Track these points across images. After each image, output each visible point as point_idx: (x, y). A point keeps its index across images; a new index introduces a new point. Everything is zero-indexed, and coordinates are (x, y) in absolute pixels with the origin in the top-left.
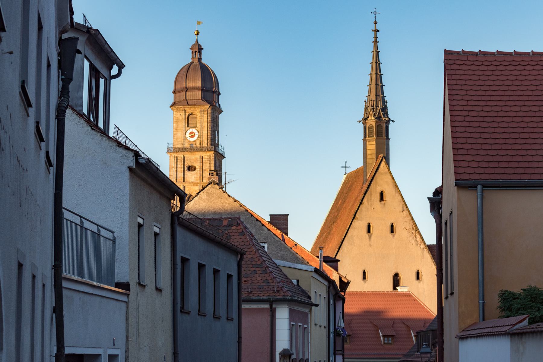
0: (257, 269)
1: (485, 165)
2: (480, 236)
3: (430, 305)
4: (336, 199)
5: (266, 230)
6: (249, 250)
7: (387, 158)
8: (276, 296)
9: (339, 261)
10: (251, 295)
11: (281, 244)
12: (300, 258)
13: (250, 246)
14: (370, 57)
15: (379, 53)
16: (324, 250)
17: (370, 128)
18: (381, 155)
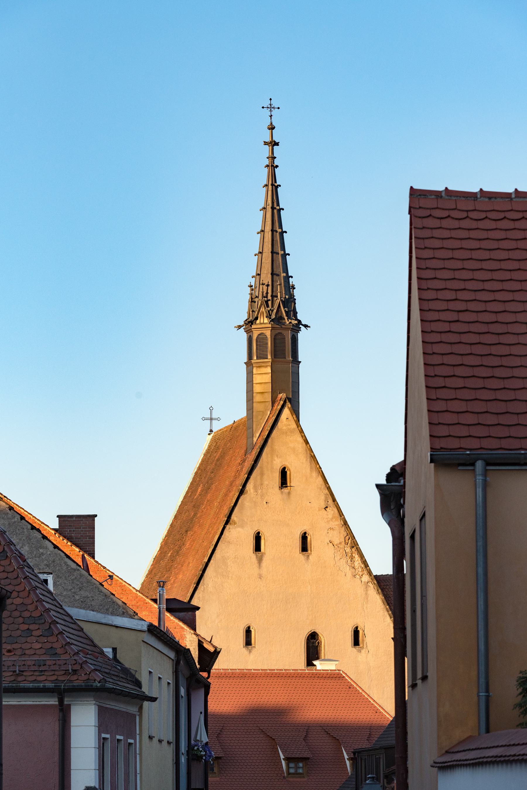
0: (32, 627)
1: (491, 420)
2: (481, 563)
3: (384, 701)
4: (192, 484)
5: (51, 547)
6: (17, 588)
7: (293, 402)
8: (71, 681)
9: (198, 608)
10: (20, 679)
11: (81, 575)
12: (120, 603)
13: (18, 581)
14: (260, 197)
15: (279, 189)
16: (168, 586)
17: (261, 338)
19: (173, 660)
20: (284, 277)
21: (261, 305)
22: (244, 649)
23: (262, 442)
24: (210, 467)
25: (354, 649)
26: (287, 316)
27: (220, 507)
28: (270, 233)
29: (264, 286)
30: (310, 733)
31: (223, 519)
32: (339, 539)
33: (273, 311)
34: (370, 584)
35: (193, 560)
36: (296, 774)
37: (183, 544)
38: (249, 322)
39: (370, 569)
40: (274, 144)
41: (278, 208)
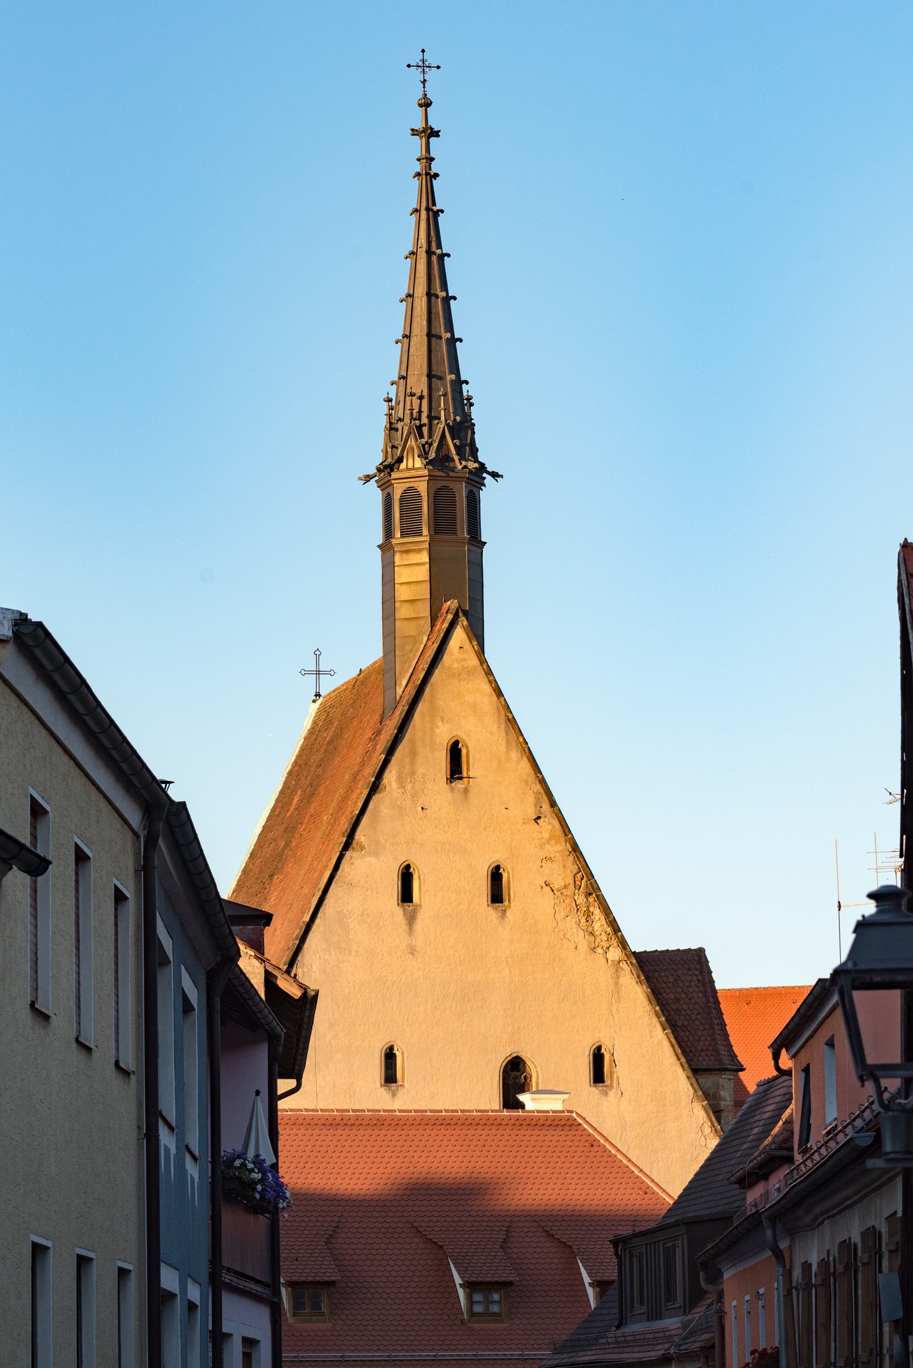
4: (282, 793)
14: (406, 232)
15: (441, 219)
18: (452, 604)
19: (135, 834)
20: (452, 381)
21: (409, 433)
22: (382, 1089)
23: (413, 693)
24: (316, 758)
25: (594, 1089)
26: (458, 454)
27: (335, 819)
28: (425, 299)
29: (414, 398)
30: (513, 1234)
31: (340, 841)
32: (564, 879)
33: (431, 445)
34: (623, 965)
35: (283, 924)
36: (487, 1315)
37: (265, 899)
38: (386, 467)
39: (622, 936)
40: (431, 133)
41: (439, 251)
